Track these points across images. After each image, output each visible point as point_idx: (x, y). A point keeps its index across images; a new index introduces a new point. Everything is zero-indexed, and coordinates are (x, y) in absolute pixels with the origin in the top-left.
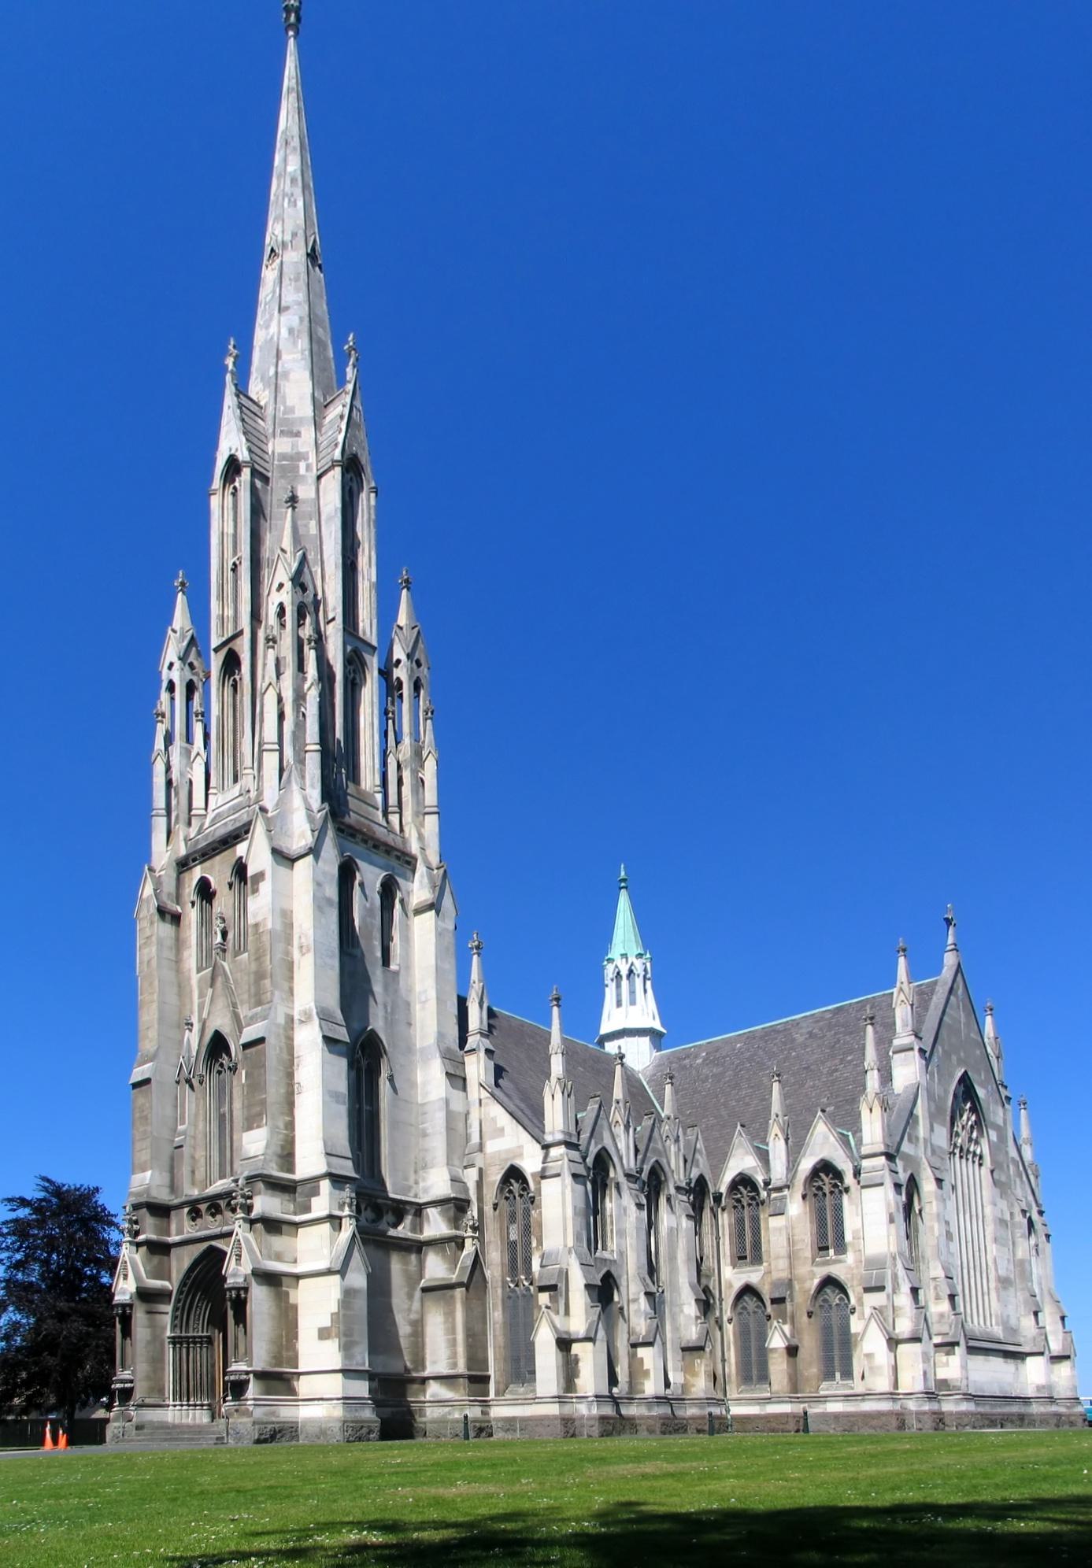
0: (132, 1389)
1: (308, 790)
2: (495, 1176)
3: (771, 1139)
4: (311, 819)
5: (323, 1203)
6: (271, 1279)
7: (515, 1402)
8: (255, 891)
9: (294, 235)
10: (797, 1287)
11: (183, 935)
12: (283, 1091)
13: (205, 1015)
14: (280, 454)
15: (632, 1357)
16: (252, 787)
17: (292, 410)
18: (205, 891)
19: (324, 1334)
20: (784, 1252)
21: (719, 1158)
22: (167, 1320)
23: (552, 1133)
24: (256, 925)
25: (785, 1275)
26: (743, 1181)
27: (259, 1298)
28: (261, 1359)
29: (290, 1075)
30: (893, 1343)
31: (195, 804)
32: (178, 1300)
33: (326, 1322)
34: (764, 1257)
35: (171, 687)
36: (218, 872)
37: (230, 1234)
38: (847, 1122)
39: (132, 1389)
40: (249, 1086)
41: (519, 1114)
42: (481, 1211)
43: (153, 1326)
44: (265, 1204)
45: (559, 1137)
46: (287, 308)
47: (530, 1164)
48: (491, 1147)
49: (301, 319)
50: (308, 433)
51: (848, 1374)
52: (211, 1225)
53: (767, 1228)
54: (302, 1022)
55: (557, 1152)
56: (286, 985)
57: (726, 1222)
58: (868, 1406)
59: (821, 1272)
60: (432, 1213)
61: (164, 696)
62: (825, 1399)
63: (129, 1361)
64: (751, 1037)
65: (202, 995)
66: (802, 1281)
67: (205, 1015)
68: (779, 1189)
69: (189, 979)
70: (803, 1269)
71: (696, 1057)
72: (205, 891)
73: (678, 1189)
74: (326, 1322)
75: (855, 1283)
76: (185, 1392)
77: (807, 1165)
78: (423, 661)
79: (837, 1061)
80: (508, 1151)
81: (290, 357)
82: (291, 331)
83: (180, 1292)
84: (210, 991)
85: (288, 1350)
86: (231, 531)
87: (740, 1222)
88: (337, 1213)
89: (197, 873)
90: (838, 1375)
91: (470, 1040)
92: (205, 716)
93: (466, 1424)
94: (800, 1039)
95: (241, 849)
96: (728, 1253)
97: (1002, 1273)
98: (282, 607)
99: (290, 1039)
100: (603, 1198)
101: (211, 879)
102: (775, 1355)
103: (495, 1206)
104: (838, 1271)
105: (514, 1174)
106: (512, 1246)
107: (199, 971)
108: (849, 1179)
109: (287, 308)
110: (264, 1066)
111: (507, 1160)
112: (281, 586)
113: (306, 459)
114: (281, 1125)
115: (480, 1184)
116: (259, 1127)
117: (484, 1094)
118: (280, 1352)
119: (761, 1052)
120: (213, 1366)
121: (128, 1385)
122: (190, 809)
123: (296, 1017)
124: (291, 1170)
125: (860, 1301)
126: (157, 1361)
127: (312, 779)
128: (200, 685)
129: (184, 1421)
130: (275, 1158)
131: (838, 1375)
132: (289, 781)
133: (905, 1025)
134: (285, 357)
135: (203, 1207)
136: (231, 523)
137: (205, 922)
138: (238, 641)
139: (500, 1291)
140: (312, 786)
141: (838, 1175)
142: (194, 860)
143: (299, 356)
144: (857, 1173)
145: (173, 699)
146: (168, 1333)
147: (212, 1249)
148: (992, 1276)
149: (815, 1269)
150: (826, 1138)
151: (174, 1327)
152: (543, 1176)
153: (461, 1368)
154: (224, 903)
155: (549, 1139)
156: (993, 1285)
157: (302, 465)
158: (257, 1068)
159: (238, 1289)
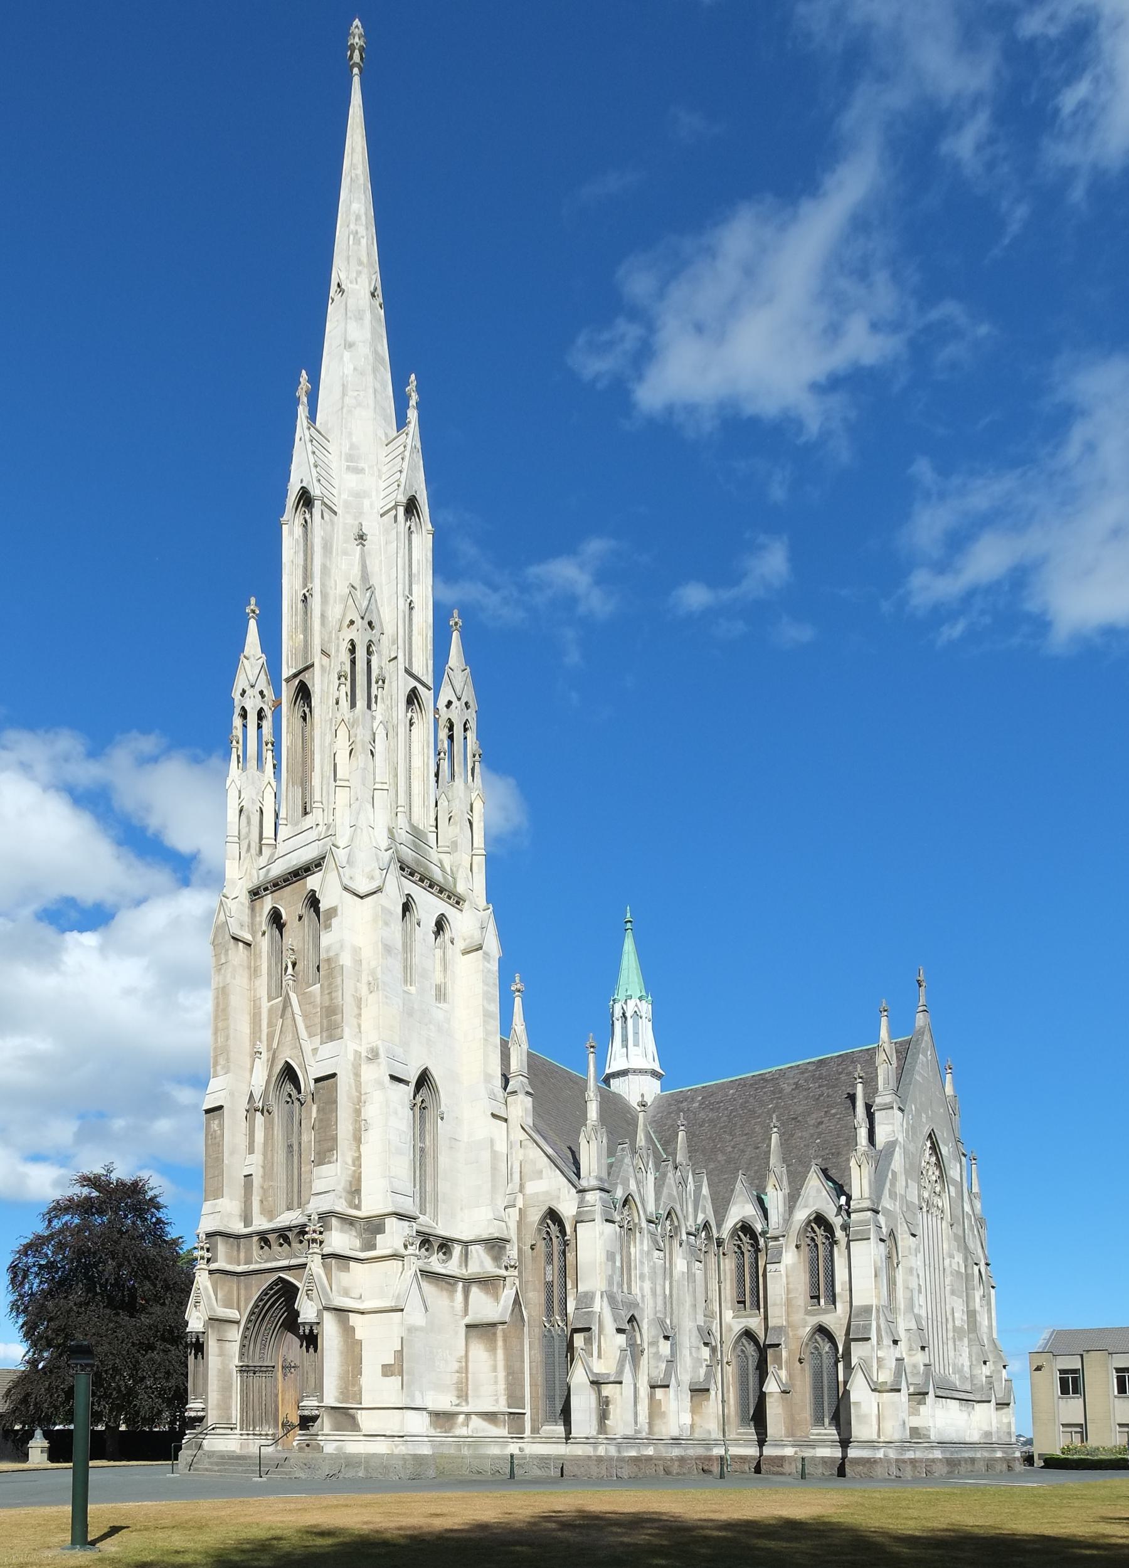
2: (535, 1216)
6: (341, 1312)
8: (328, 927)
13: (275, 1046)
15: (652, 1397)
18: (276, 919)
21: (721, 1207)
22: (235, 1348)
24: (328, 960)
27: (330, 1332)
28: (331, 1397)
29: (358, 1112)
32: (247, 1329)
35: (244, 714)
36: (290, 904)
37: (303, 1266)
41: (559, 1161)
42: (520, 1250)
43: (222, 1354)
44: (339, 1240)
45: (594, 1183)
47: (568, 1209)
48: (531, 1187)
55: (592, 1197)
56: (355, 1021)
59: (813, 1321)
60: (477, 1251)
61: (237, 722)
62: (812, 1445)
63: (200, 1390)
64: (742, 1083)
65: (270, 1024)
67: (275, 1046)
68: (776, 1239)
71: (693, 1100)
72: (276, 919)
73: (688, 1234)
76: (249, 1422)
77: (802, 1215)
78: (471, 704)
83: (249, 1321)
85: (353, 1385)
87: (740, 1268)
88: (402, 1251)
89: (268, 903)
92: (276, 745)
93: (512, 1463)
94: (787, 1089)
95: (312, 882)
96: (729, 1298)
97: (958, 1323)
100: (629, 1243)
105: (553, 1215)
106: (549, 1285)
107: (270, 999)
110: (336, 1102)
112: (352, 622)
114: (350, 1162)
115: (520, 1223)
117: (523, 1136)
118: (346, 1388)
119: (751, 1100)
121: (201, 1414)
122: (261, 838)
124: (358, 1207)
126: (226, 1389)
128: (268, 713)
130: (344, 1194)
135: (272, 1237)
137: (278, 952)
142: (266, 889)
145: (245, 726)
146: (237, 1362)
148: (950, 1326)
151: (242, 1355)
153: (502, 1406)
154: (294, 935)
155: (584, 1183)
156: (951, 1335)
157: (366, 503)
158: (329, 1105)
159: (311, 1325)
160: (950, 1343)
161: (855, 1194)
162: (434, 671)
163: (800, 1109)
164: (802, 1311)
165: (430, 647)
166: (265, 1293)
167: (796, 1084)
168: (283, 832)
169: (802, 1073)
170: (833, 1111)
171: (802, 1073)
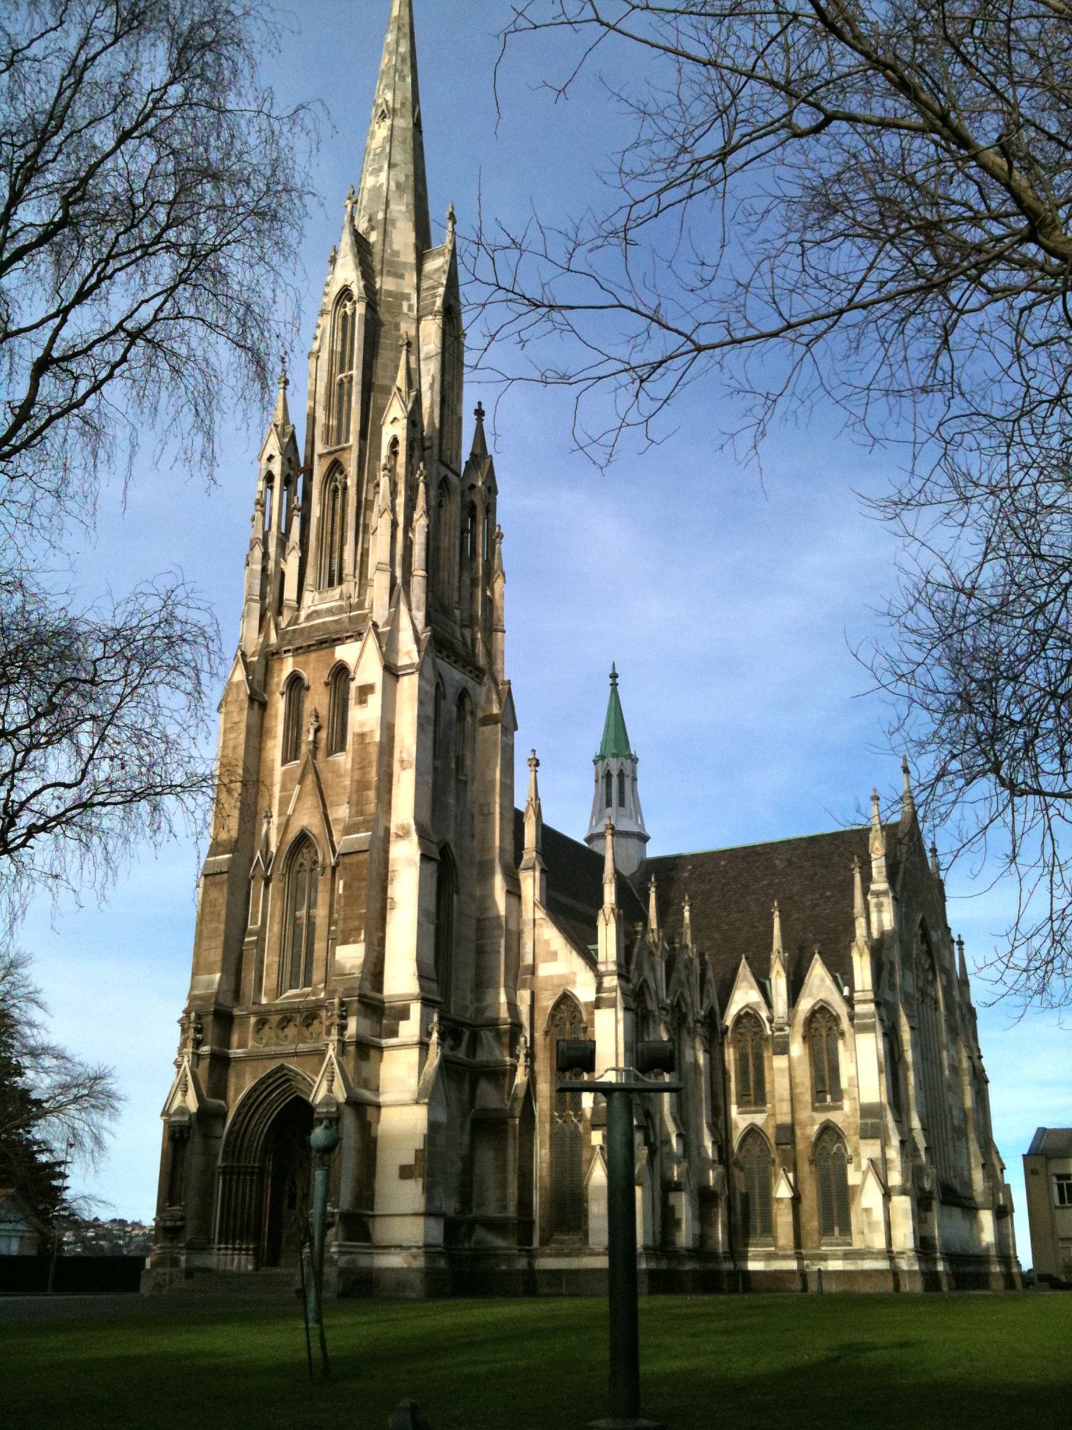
0: (183, 1227)
1: (414, 612)
2: (547, 1001)
3: (773, 975)
4: (417, 640)
5: (410, 1029)
7: (558, 1254)
9: (403, 104)
10: (798, 1132)
11: (267, 724)
12: (378, 906)
13: (289, 812)
14: (387, 291)
16: (355, 594)
17: (397, 254)
19: (406, 1172)
20: (786, 1094)
23: (606, 963)
25: (787, 1119)
26: (748, 1017)
30: (887, 1194)
31: (286, 595)
33: (409, 1159)
34: (768, 1098)
38: (841, 971)
39: (183, 1227)
40: (347, 897)
46: (395, 165)
49: (407, 176)
50: (411, 278)
51: (846, 1229)
52: (291, 1041)
53: (771, 1068)
54: (398, 836)
57: (732, 1058)
58: (868, 1265)
59: (821, 1118)
62: (824, 1258)
65: (283, 789)
66: (804, 1126)
67: (289, 812)
69: (273, 770)
70: (805, 1114)
74: (409, 1159)
75: (852, 1132)
79: (817, 896)
80: (561, 977)
81: (397, 208)
82: (398, 185)
84: (298, 787)
86: (339, 349)
90: (836, 1229)
91: (525, 857)
98: (395, 442)
99: (386, 852)
101: (304, 674)
102: (782, 1206)
103: (546, 1033)
104: (835, 1117)
108: (845, 1024)
109: (395, 165)
111: (559, 986)
113: (409, 300)
116: (355, 942)
120: (261, 1203)
121: (179, 1223)
123: (393, 830)
125: (856, 1150)
127: (418, 602)
129: (228, 1268)
130: (369, 977)
131: (836, 1229)
132: (398, 602)
133: (879, 873)
134: (393, 206)
136: (339, 343)
138: (346, 455)
139: (548, 1127)
140: (418, 609)
141: (836, 1019)
143: (403, 208)
144: (851, 1018)
146: (219, 1163)
147: (282, 1067)
149: (816, 1115)
150: (822, 980)
152: (598, 1004)
160: (950, 1144)
161: (858, 986)
162: (88, 1289)
163: (796, 889)
164: (810, 1106)
165: (378, 1153)
166: (261, 1082)
167: (789, 860)
168: (308, 597)
169: (795, 849)
170: (828, 894)
171: (795, 849)
